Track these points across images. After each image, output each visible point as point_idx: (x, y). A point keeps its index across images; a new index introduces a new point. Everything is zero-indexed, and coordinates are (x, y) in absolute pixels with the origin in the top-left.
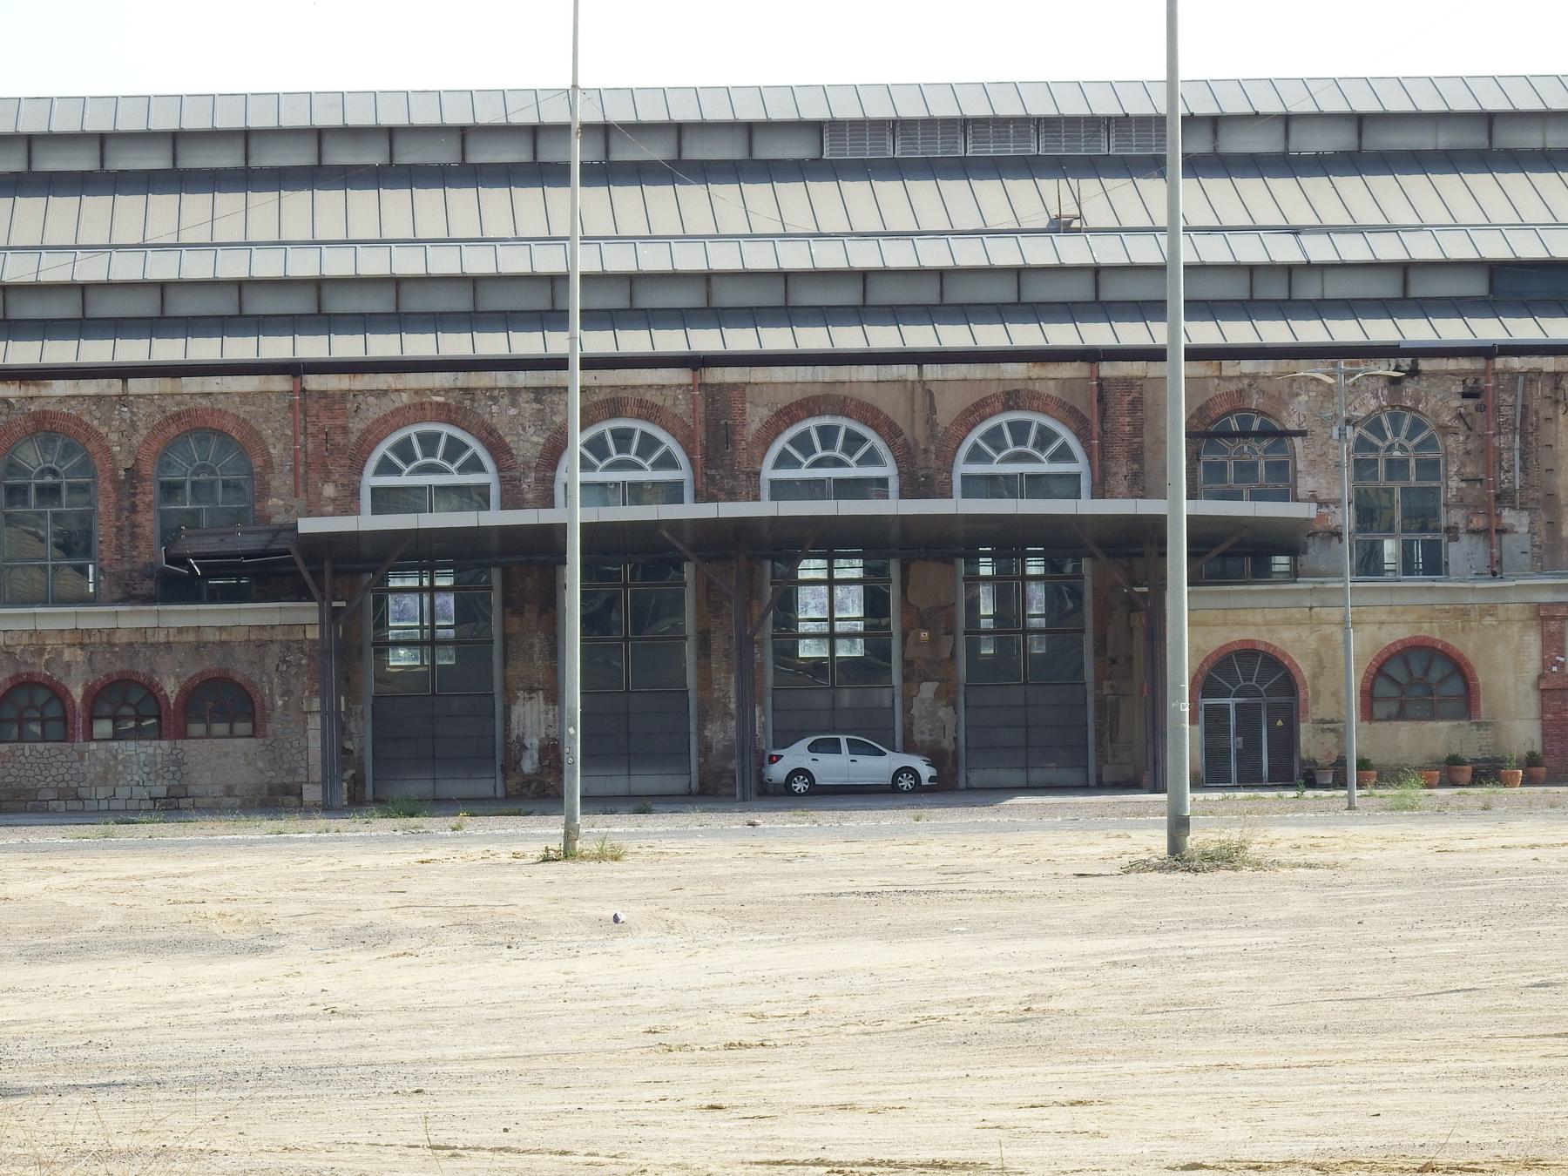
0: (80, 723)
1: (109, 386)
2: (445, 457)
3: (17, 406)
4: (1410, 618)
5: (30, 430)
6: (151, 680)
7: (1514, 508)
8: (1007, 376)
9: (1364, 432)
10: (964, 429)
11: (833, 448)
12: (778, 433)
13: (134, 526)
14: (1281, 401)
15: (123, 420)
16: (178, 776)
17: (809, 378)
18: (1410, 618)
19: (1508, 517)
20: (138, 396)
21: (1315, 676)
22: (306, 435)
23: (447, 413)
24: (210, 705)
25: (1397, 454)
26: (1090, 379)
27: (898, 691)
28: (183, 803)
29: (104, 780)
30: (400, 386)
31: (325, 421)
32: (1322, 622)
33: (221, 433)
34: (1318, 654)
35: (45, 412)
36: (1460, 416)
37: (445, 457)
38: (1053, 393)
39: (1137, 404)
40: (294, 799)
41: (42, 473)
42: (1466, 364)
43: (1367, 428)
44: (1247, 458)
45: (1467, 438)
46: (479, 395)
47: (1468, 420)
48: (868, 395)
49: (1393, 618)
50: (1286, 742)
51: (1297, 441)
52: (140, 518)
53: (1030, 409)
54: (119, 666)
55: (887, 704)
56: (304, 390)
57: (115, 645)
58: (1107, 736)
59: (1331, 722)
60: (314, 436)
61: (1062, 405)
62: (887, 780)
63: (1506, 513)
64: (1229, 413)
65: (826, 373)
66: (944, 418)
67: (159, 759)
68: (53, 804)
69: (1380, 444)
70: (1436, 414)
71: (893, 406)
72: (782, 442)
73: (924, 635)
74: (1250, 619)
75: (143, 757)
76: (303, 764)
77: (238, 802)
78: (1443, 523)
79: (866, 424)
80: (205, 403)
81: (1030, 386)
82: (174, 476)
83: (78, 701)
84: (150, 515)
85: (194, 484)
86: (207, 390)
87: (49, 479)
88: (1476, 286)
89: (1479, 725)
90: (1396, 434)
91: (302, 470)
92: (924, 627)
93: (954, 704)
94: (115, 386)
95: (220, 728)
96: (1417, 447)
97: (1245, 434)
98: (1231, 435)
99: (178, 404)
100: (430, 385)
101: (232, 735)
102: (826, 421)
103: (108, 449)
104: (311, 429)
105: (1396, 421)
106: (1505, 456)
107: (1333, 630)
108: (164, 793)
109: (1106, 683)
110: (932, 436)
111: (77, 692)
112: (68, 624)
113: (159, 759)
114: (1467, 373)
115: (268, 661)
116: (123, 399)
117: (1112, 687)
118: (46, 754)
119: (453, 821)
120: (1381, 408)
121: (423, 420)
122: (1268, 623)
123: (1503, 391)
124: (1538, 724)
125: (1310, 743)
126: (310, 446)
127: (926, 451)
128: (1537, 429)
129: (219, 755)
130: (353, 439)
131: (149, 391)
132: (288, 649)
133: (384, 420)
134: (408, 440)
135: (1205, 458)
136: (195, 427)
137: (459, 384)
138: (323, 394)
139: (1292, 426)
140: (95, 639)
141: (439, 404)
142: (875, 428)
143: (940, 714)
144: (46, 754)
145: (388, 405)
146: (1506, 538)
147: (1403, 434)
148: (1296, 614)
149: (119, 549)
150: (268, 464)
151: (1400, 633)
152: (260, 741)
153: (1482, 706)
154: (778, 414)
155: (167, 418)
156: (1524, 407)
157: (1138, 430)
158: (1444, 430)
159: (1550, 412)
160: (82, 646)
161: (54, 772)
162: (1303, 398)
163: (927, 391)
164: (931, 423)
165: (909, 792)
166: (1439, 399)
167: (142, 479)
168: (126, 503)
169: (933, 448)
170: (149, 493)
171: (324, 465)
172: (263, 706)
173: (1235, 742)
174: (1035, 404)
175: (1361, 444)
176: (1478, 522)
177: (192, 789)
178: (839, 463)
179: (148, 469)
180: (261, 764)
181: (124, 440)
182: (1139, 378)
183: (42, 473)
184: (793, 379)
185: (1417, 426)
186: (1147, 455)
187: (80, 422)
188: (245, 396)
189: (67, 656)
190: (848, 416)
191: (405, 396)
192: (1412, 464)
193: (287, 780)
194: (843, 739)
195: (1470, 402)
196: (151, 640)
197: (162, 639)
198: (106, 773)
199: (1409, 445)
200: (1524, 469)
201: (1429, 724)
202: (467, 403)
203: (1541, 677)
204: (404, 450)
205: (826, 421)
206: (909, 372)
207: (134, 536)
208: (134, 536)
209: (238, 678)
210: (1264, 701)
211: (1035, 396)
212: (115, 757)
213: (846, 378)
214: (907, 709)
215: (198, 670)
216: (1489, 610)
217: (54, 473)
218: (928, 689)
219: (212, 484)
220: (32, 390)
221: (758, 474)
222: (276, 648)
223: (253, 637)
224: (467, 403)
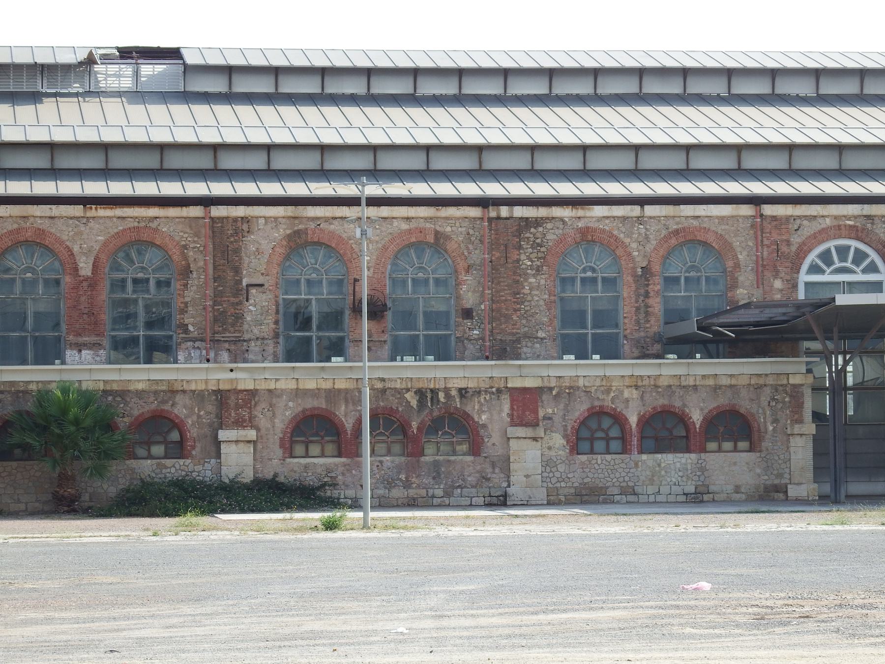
0: (635, 441)
1: (632, 210)
2: (853, 262)
3: (569, 223)
5: (578, 240)
6: (683, 411)
13: (647, 306)
15: (640, 234)
16: (702, 478)
20: (651, 218)
22: (762, 245)
23: (856, 233)
24: (722, 429)
28: (706, 497)
29: (652, 481)
30: (825, 213)
31: (775, 236)
33: (705, 244)
35: (588, 228)
37: (853, 262)
40: (781, 496)
41: (584, 270)
46: (877, 220)
52: (651, 301)
54: (662, 401)
56: (762, 215)
57: (659, 387)
60: (768, 247)
67: (689, 467)
68: (617, 498)
75: (678, 465)
76: (787, 471)
77: (744, 497)
80: (695, 223)
82: (672, 272)
83: (634, 426)
84: (658, 300)
85: (686, 278)
86: (697, 214)
87: (589, 274)
91: (760, 269)
94: (635, 211)
95: (727, 445)
99: (677, 223)
100: (845, 213)
101: (735, 450)
103: (630, 254)
104: (766, 242)
108: (693, 490)
111: (633, 420)
112: (627, 372)
113: (689, 467)
115: (763, 398)
116: (640, 219)
118: (612, 463)
121: (840, 237)
126: (765, 253)
129: (730, 465)
130: (794, 248)
131: (658, 214)
132: (777, 390)
133: (814, 236)
134: (828, 251)
136: (688, 239)
137: (865, 213)
138: (774, 218)
140: (646, 382)
141: (850, 226)
144: (612, 463)
145: (816, 226)
149: (638, 322)
150: (737, 266)
152: (758, 454)
155: (670, 233)
160: (637, 387)
161: (618, 475)
167: (652, 275)
168: (642, 291)
170: (656, 285)
171: (775, 266)
172: (759, 431)
177: (712, 488)
179: (656, 267)
180: (758, 471)
181: (641, 248)
183: (584, 270)
187: (611, 235)
188: (722, 219)
189: (626, 394)
191: (828, 220)
193: (776, 482)
196: (684, 384)
197: (692, 383)
198: (653, 476)
202: (869, 226)
204: (826, 257)
207: (647, 314)
208: (647, 314)
209: (742, 411)
212: (659, 465)
215: (716, 405)
217: (593, 270)
219: (699, 279)
220: (580, 212)
222: (768, 391)
223: (753, 382)
224: (869, 226)
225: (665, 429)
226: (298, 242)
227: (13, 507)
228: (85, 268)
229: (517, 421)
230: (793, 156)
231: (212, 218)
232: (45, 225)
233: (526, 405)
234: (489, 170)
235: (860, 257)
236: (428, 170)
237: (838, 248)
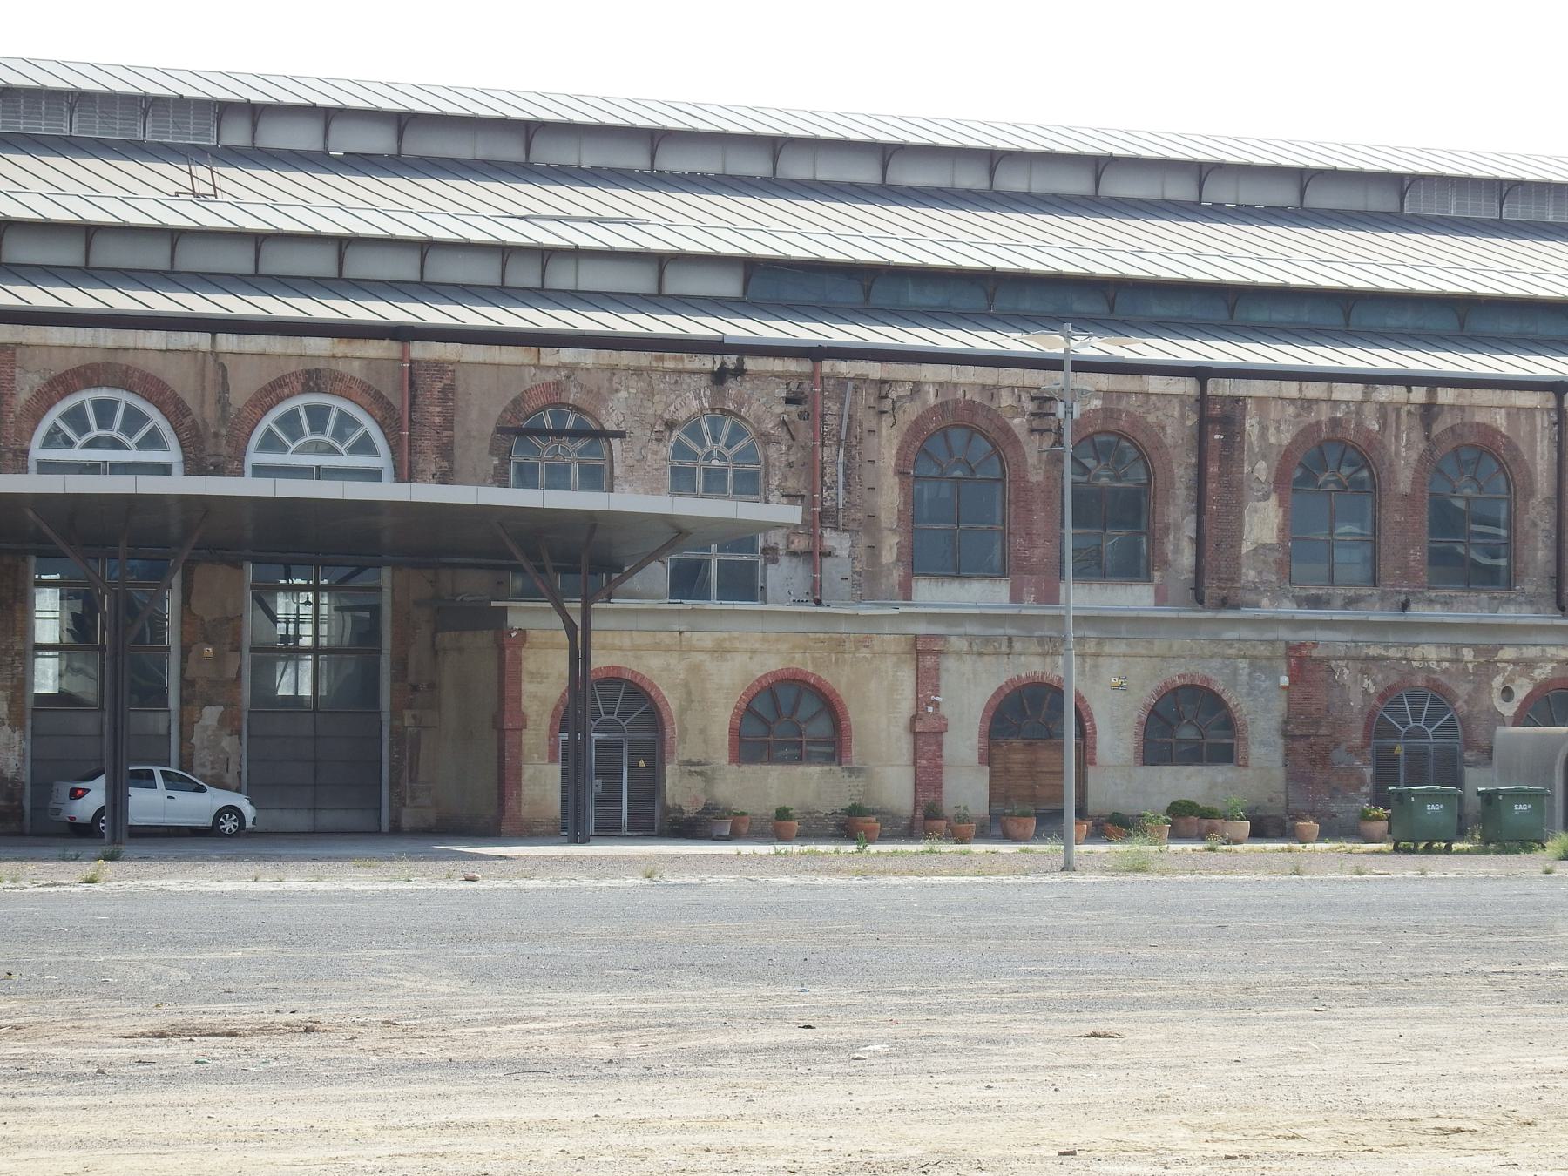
4: (784, 647)
7: (836, 529)
8: (309, 352)
9: (683, 437)
10: (258, 411)
11: (110, 427)
12: (50, 406)
14: (599, 396)
17: (89, 342)
18: (784, 647)
19: (831, 539)
21: (683, 711)
25: (715, 462)
26: (402, 360)
27: (175, 716)
32: (692, 649)
34: (686, 685)
36: (784, 423)
38: (358, 376)
39: (448, 392)
42: (792, 366)
43: (685, 433)
44: (559, 460)
45: (790, 448)
47: (792, 427)
48: (155, 366)
49: (766, 647)
50: (649, 785)
51: (615, 442)
53: (332, 393)
55: (163, 731)
58: (406, 774)
59: (699, 764)
61: (367, 389)
62: (207, 821)
63: (827, 534)
64: (543, 409)
65: (109, 337)
66: (239, 396)
69: (699, 451)
70: (759, 420)
71: (180, 379)
72: (52, 417)
73: (208, 651)
74: (617, 642)
78: (761, 544)
79: (149, 400)
81: (333, 365)
88: (730, 286)
89: (851, 771)
90: (715, 440)
92: (210, 643)
93: (239, 733)
96: (736, 456)
97: (559, 433)
98: (543, 433)
102: (104, 393)
105: (715, 424)
106: (828, 470)
107: (699, 663)
109: (407, 713)
110: (224, 418)
114: (792, 375)
117: (414, 717)
119: (87, 869)
120: (701, 410)
122: (636, 648)
123: (830, 398)
124: (911, 769)
125: (679, 790)
127: (216, 435)
128: (860, 442)
135: (517, 457)
139: (610, 426)
142: (160, 407)
143: (224, 744)
146: (827, 562)
147: (723, 441)
148: (665, 638)
151: (773, 664)
153: (854, 749)
154: (51, 384)
156: (850, 417)
157: (448, 423)
158: (767, 439)
159: (873, 424)
162: (623, 394)
163: (219, 364)
164: (223, 403)
165: (231, 835)
166: (762, 403)
169: (223, 432)
173: (595, 785)
174: (338, 386)
175: (680, 450)
176: (800, 544)
178: (116, 444)
182: (451, 363)
184: (71, 342)
185: (737, 433)
186: (457, 452)
190: (130, 390)
192: (731, 475)
194: (157, 770)
195: (793, 408)
199: (729, 454)
200: (847, 486)
201: (800, 769)
203: (914, 719)
204: (290, 422)
205: (104, 393)
206: (202, 340)
210: (626, 737)
211: (338, 377)
213: (131, 344)
214: (185, 737)
216: (864, 642)
218: (211, 715)
221: (26, 452)
230: (262, 255)
231: (412, 362)
232: (1500, 421)
234: (270, 276)
236: (256, 275)
237: (130, 410)
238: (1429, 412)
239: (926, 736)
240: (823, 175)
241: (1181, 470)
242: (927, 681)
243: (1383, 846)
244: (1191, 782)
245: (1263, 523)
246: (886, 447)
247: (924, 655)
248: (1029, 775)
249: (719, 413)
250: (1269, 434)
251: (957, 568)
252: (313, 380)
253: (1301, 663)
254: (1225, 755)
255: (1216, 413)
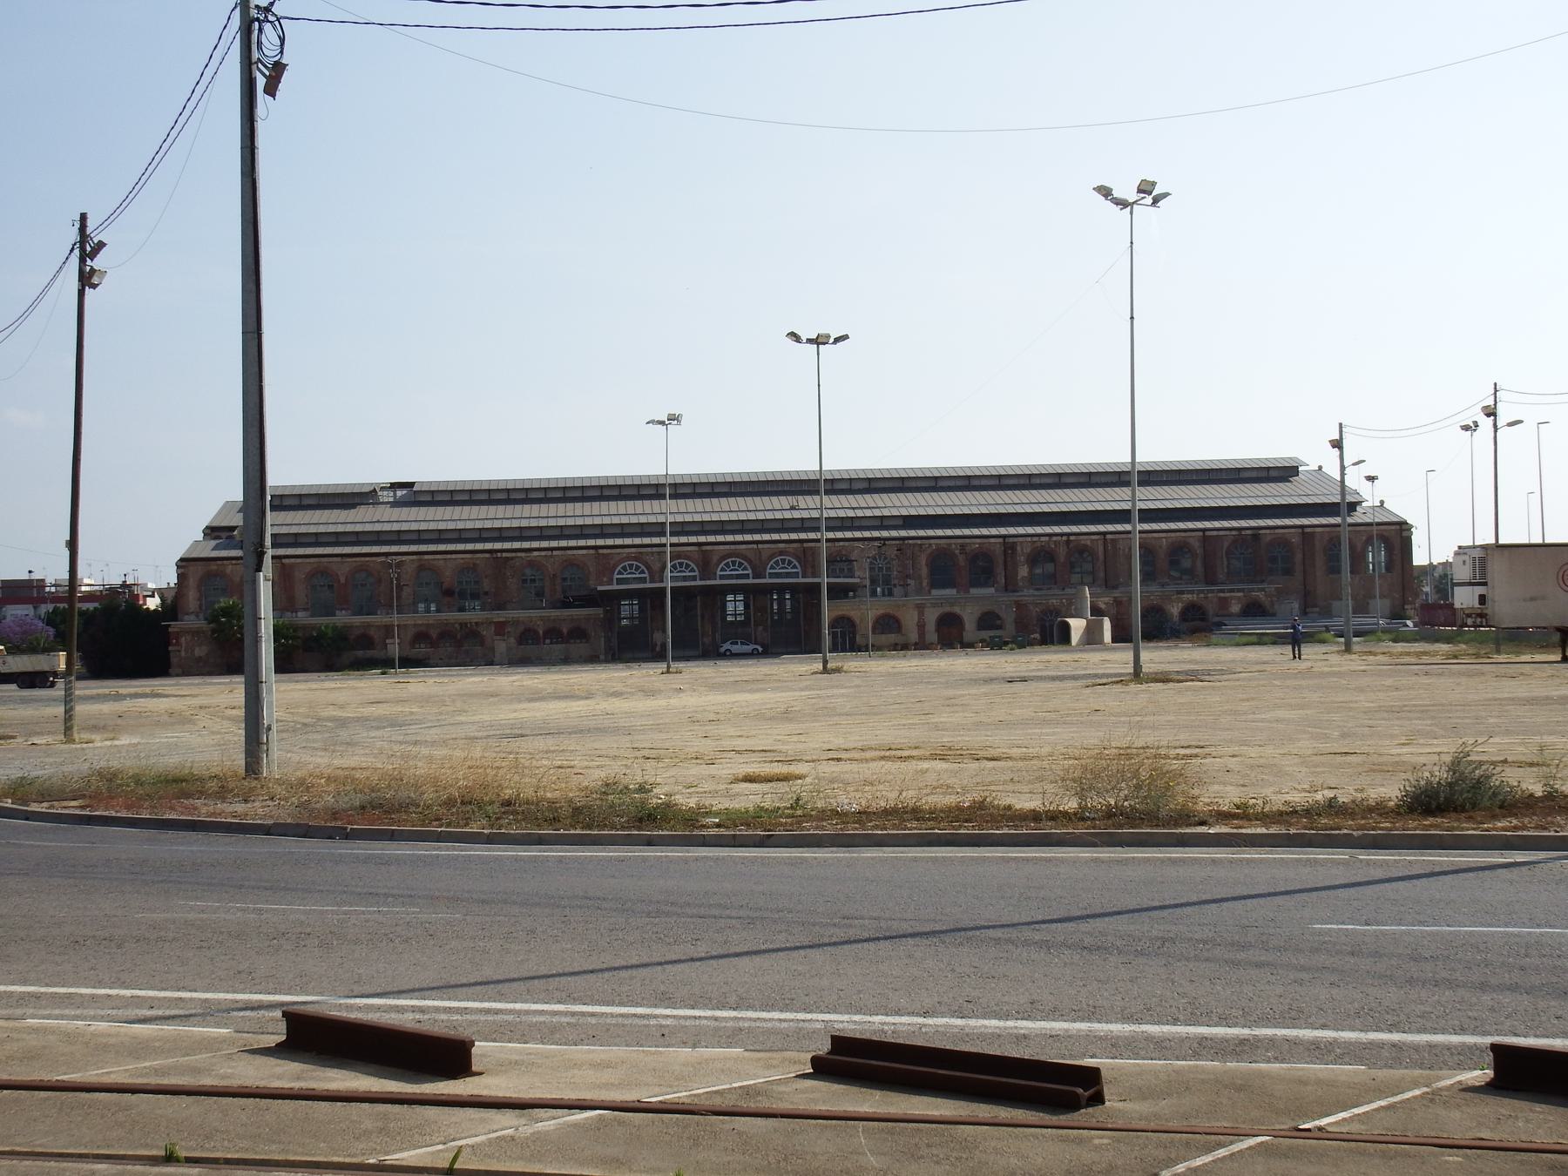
23: (636, 559)
107: (866, 611)
129: (579, 648)
136: (570, 564)
204: (624, 568)
225: (553, 634)
226: (421, 568)
227: (1382, 1114)
228: (343, 580)
229: (497, 633)
233: (500, 628)
235: (638, 568)
238: (1068, 542)
239: (921, 627)
240: (785, 501)
241: (1000, 560)
242: (921, 614)
243: (1552, 658)
244: (986, 634)
245: (1023, 571)
246: (923, 560)
247: (920, 608)
248: (950, 636)
249: (880, 555)
250: (1023, 551)
251: (944, 586)
252: (781, 553)
253: (1019, 605)
254: (1000, 627)
255: (1009, 545)
